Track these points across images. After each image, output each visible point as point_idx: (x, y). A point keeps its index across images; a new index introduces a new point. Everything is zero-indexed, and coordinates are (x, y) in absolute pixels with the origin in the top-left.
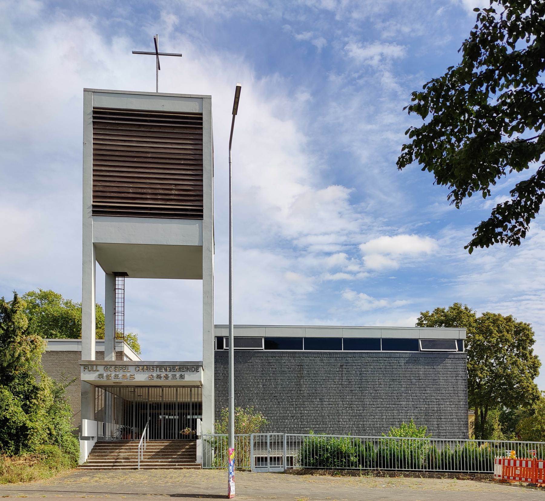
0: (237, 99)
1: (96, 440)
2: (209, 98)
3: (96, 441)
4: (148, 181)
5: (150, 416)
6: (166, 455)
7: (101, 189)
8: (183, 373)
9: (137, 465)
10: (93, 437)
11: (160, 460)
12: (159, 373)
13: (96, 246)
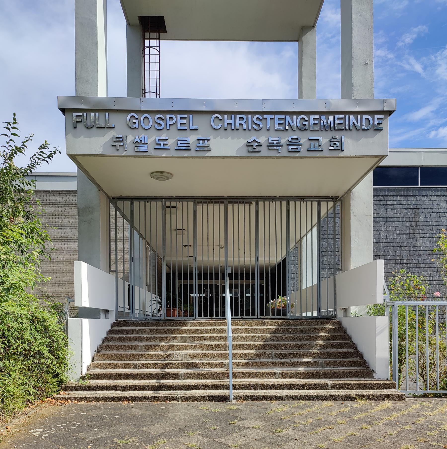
1: (112, 318)
6: (285, 355)
8: (338, 135)
11: (278, 370)
12: (273, 137)
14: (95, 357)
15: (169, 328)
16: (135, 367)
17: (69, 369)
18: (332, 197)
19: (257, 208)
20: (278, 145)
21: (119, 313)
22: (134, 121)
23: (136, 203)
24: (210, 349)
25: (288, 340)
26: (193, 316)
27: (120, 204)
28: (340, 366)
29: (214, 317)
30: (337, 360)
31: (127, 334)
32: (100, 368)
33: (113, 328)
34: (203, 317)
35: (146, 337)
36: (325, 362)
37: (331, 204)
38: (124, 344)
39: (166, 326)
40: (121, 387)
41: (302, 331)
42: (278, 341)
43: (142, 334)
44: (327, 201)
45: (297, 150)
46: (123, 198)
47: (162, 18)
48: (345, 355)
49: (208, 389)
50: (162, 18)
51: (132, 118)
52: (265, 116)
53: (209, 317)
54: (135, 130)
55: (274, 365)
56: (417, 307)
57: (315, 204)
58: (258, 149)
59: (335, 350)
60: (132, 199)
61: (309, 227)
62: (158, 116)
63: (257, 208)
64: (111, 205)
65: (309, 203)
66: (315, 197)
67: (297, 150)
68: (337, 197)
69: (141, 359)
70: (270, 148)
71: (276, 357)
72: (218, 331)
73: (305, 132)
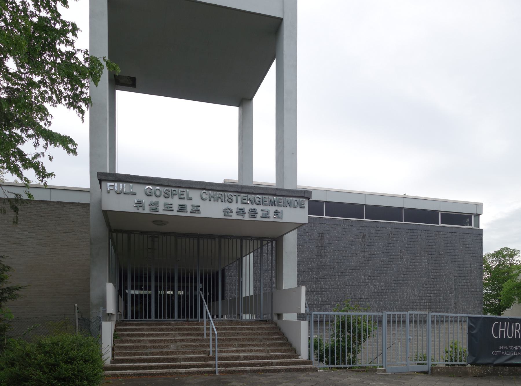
5: (201, 282)
6: (244, 345)
8: (279, 209)
11: (242, 355)
12: (241, 206)
17: (13, 365)
18: (270, 238)
19: (220, 243)
23: (132, 236)
24: (193, 342)
25: (244, 336)
29: (189, 319)
30: (276, 348)
34: (139, 319)
36: (270, 350)
41: (252, 329)
47: (135, 78)
50: (135, 78)
52: (235, 194)
53: (185, 319)
55: (238, 351)
58: (230, 214)
59: (275, 342)
61: (248, 252)
63: (220, 243)
66: (260, 238)
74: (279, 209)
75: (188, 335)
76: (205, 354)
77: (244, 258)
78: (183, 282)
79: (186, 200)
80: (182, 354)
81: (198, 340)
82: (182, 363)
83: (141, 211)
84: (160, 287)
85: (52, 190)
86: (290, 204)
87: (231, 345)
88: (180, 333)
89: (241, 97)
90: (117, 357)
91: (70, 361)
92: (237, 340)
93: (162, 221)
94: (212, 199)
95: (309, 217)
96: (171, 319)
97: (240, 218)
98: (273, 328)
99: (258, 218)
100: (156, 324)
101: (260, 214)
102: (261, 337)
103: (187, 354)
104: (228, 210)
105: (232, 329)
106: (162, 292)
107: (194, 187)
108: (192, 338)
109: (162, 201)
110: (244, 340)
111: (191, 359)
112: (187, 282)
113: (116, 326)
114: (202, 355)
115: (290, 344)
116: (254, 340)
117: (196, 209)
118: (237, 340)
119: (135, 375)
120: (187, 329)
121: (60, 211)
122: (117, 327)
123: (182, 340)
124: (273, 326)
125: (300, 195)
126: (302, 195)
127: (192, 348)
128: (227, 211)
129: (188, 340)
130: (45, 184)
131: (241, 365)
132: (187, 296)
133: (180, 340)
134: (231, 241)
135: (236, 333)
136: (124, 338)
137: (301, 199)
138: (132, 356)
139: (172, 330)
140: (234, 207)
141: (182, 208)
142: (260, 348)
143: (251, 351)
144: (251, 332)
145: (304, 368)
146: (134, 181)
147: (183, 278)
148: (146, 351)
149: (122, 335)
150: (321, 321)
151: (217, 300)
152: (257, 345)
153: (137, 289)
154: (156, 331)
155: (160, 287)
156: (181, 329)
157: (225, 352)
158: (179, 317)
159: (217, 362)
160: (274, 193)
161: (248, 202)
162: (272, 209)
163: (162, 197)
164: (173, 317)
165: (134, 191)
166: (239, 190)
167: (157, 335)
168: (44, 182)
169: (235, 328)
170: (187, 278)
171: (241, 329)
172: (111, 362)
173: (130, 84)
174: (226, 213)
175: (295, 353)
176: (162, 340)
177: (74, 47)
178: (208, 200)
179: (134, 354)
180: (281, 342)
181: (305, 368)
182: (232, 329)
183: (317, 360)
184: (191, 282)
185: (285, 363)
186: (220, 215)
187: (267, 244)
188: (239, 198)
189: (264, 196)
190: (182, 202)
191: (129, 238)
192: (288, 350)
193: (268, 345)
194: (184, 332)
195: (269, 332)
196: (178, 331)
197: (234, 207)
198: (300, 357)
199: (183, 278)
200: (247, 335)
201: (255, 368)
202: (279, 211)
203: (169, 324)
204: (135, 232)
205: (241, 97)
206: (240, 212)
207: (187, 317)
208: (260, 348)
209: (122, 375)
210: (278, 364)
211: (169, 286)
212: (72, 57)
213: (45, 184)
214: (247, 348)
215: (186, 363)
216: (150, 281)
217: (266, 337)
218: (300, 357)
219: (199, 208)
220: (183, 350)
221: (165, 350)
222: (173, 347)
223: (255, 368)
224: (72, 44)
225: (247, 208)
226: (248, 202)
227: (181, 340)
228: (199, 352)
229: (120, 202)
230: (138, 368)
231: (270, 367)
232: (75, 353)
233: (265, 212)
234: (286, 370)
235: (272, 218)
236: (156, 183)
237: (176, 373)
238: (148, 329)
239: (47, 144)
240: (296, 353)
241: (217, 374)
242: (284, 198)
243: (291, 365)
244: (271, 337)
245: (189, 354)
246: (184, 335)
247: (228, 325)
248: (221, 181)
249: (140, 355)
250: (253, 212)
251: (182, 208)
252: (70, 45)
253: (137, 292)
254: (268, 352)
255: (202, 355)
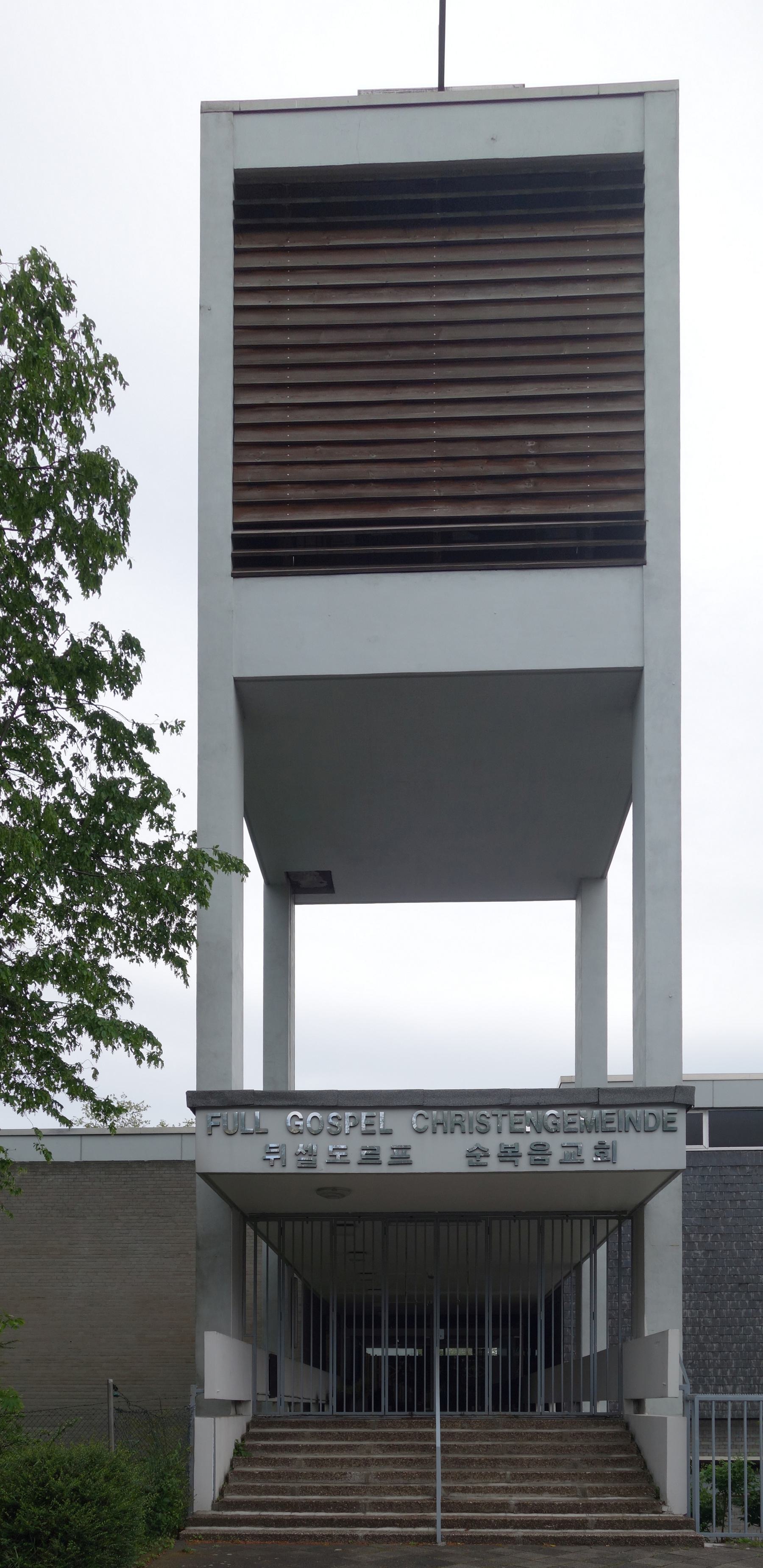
0: (213, 1102)
1: (248, 1412)
2: (669, 91)
3: (249, 1418)
4: (435, 432)
5: (443, 1325)
6: (528, 1477)
7: (268, 475)
8: (608, 1139)
9: (431, 1523)
10: (237, 1403)
11: (515, 1499)
12: (509, 1140)
13: (244, 688)
14: (230, 1477)
15: (341, 1430)
16: (293, 1492)
18: (615, 1212)
19: (488, 1231)
20: (514, 1154)
21: (258, 1405)
22: (297, 1123)
23: (288, 1225)
24: (408, 1466)
25: (536, 1453)
26: (380, 1410)
27: (262, 1225)
28: (613, 1495)
29: (415, 1412)
31: (275, 1440)
32: (239, 1494)
33: (252, 1430)
35: (306, 1446)
36: (589, 1488)
37: (614, 1223)
38: (273, 1456)
39: (336, 1427)
40: (275, 1521)
41: (560, 1437)
42: (518, 1453)
43: (299, 1440)
44: (607, 1219)
45: (543, 1162)
46: (266, 1217)
48: (624, 1477)
49: (405, 1527)
51: (295, 1118)
53: (406, 1413)
54: (299, 1135)
55: (506, 1490)
56: (730, 1404)
57: (586, 1223)
58: (483, 1160)
59: (609, 1470)
60: (281, 1218)
62: (334, 1114)
63: (488, 1231)
64: (248, 1227)
65: (577, 1223)
66: (587, 1212)
67: (543, 1162)
68: (625, 1212)
69: (301, 1480)
70: (501, 1159)
71: (513, 1479)
72: (421, 1436)
73: (556, 1135)
74: (608, 1139)
75: (400, 1448)
76: (427, 1494)
77: (586, 1264)
78: (401, 1326)
79: (378, 1136)
80: (373, 1494)
81: (419, 1461)
82: (369, 1514)
83: (277, 1169)
84: (368, 1338)
85: (185, 1137)
86: (631, 1124)
87: (493, 1475)
88: (380, 1445)
89: (578, 879)
90: (229, 1497)
91: (43, 1499)
92: (513, 1462)
93: (334, 1189)
94: (440, 1129)
95: (689, 1154)
96: (373, 1413)
97: (508, 1167)
98: (614, 1435)
99: (554, 1166)
100: (336, 1424)
101: (557, 1154)
102: (576, 1458)
103: (385, 1494)
104: (478, 1152)
105: (509, 1436)
106: (418, 1352)
107: (395, 1104)
108: (405, 1456)
109: (556, 1143)
110: (530, 1462)
111: (390, 1506)
112: (463, 1325)
113: (248, 1427)
114: (420, 1498)
115: (650, 1478)
116: (556, 1463)
117: (402, 1156)
118: (513, 1462)
119: (254, 1536)
120: (403, 1436)
121: (132, 1183)
122: (252, 1430)
123: (382, 1460)
124: (617, 1429)
125: (661, 1100)
126: (668, 1099)
127: (401, 1480)
128: (476, 1155)
129: (395, 1461)
130: (112, 1127)
131: (505, 1524)
132: (505, 1359)
133: (378, 1460)
134: (567, 1225)
135: (514, 1447)
136: (255, 1455)
137: (667, 1110)
138: (261, 1494)
139: (367, 1437)
140: (492, 1142)
141: (372, 1156)
142: (568, 1484)
143: (540, 1491)
144: (557, 1443)
145: (666, 1538)
146: (263, 1104)
147: (401, 1317)
148: (291, 1485)
149: (254, 1448)
150: (721, 1421)
151: (534, 1369)
152: (562, 1477)
153: (402, 1346)
154: (330, 1439)
155: (368, 1338)
156: (387, 1436)
157: (475, 1490)
158: (495, 1408)
159: (438, 1515)
160: (594, 1099)
161: (528, 1129)
162: (588, 1142)
163: (324, 1134)
164: (378, 1408)
165: (388, 1127)
166: (506, 1101)
167: (329, 1449)
168: (109, 1123)
169: (518, 1434)
170: (411, 1317)
171: (533, 1437)
172: (214, 1507)
173: (323, 888)
174: (474, 1160)
175: (657, 1496)
176: (336, 1460)
177: (174, 830)
178: (430, 1131)
179: (267, 1491)
180: (627, 1469)
181: (671, 1538)
182: (509, 1436)
183: (743, 1519)
184: (472, 1326)
185: (619, 1521)
186: (460, 1166)
187: (619, 1226)
188: (505, 1122)
189: (567, 1111)
190: (370, 1142)
191: (281, 1231)
192: (638, 1491)
193: (588, 1477)
194: (395, 1443)
195: (600, 1444)
196: (382, 1439)
197: (492, 1142)
198: (664, 1508)
199: (401, 1317)
200: (544, 1450)
201: (538, 1532)
202: (608, 1143)
203: (363, 1424)
204: (294, 1217)
205: (578, 879)
206: (509, 1154)
207: (411, 1409)
208: (568, 1484)
209: (226, 1536)
210: (599, 1524)
211: (463, 1337)
212: (167, 852)
213: (112, 1127)
214: (535, 1484)
215: (376, 1514)
216: (378, 1325)
217: (591, 1456)
218: (664, 1508)
219: (409, 1152)
220: (378, 1483)
221: (332, 1484)
222: (356, 1476)
223: (538, 1532)
224: (170, 825)
225: (524, 1144)
226: (528, 1129)
227: (379, 1462)
228: (414, 1491)
229: (236, 1154)
230: (266, 1522)
231: (580, 1533)
232: (59, 1483)
233: (572, 1149)
234: (617, 1541)
235: (590, 1162)
236: (310, 1103)
237: (344, 1536)
238: (314, 1436)
239: (98, 1046)
240: (658, 1498)
241: (440, 1543)
242: (621, 1110)
243: (635, 1528)
244: (605, 1457)
245: (389, 1494)
246: (391, 1448)
247: (504, 1427)
248: (555, 1085)
249: (278, 1494)
250: (540, 1151)
251: (372, 1156)
252: (166, 827)
253: (402, 1352)
254: (584, 1495)
255: (420, 1498)
